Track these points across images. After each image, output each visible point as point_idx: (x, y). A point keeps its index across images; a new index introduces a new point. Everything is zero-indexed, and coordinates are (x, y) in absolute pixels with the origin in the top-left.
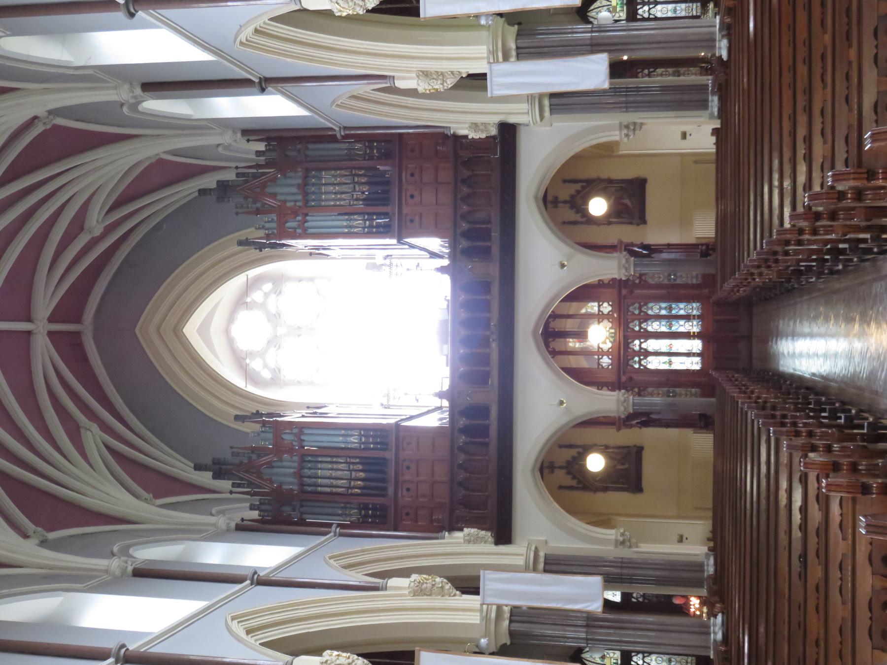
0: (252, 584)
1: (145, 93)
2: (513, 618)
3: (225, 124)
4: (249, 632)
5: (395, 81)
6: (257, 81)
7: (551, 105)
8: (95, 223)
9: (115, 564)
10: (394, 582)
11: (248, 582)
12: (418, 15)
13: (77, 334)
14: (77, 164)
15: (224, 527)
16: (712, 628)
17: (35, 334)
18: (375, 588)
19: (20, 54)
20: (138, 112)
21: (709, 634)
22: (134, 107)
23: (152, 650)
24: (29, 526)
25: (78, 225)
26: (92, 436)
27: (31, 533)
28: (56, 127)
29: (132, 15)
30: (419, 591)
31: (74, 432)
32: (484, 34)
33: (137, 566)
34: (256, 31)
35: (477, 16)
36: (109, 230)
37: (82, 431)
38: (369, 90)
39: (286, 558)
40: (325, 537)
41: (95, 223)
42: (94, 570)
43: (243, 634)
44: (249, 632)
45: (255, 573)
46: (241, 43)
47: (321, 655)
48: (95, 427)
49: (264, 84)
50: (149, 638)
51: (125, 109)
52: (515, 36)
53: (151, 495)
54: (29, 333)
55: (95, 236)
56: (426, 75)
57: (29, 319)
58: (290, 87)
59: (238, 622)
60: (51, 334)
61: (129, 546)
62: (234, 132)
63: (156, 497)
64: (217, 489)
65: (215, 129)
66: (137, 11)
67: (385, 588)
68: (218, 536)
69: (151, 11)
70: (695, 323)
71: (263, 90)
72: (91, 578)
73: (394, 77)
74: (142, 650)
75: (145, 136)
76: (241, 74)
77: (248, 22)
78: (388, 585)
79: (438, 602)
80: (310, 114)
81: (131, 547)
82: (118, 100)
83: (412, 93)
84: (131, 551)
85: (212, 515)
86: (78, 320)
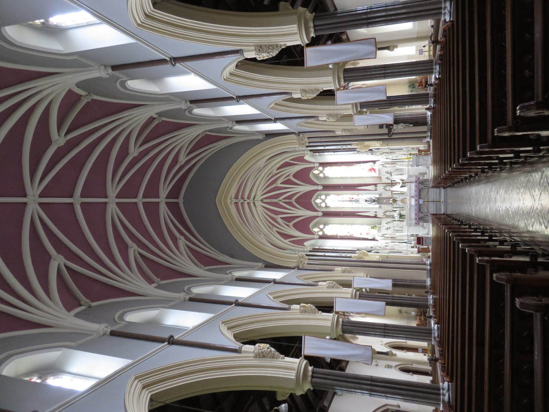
0: (168, 344)
1: (114, 72)
2: (343, 324)
3: (261, 132)
4: (274, 298)
5: (244, 53)
6: (273, 119)
7: (344, 77)
8: (182, 159)
9: (182, 295)
10: (320, 283)
11: (234, 305)
12: (304, 65)
13: (177, 203)
14: (174, 135)
15: (261, 266)
16: (433, 331)
17: (109, 204)
18: (315, 286)
19: (41, 47)
20: (192, 114)
21: (431, 333)
22: (190, 112)
23: (183, 339)
24: (200, 264)
25: (175, 160)
26: (182, 241)
27: (82, 303)
28: (206, 135)
29: (238, 102)
30: (304, 311)
31: (175, 240)
32: (331, 72)
33: (113, 329)
34: (275, 104)
35: (328, 65)
36: (188, 162)
37: (178, 240)
38: (280, 101)
39: (121, 367)
40: (294, 270)
41: (182, 159)
42: (173, 298)
43: (272, 298)
44: (274, 298)
45: (237, 300)
46: (225, 79)
47: (300, 305)
48: (182, 238)
49: (276, 120)
50: (188, 331)
51: (186, 113)
52: (343, 72)
53: (159, 279)
54: (106, 203)
55: (60, 145)
56: (304, 91)
57: (106, 197)
58: (249, 100)
59: (225, 324)
60: (167, 203)
61: (191, 287)
62: (186, 101)
63: (205, 266)
64: (196, 275)
65: (94, 66)
66: (176, 64)
67: (317, 285)
68: (260, 269)
69: (182, 63)
70: (318, 201)
71: (275, 122)
72: (223, 281)
73: (291, 93)
74: (179, 339)
75: (201, 124)
76: (269, 117)
77: (272, 102)
78: (242, 350)
79: (311, 316)
80: (135, 42)
81: (124, 315)
82: (99, 76)
83: (299, 101)
84: (232, 273)
85: (227, 274)
86: (177, 198)
